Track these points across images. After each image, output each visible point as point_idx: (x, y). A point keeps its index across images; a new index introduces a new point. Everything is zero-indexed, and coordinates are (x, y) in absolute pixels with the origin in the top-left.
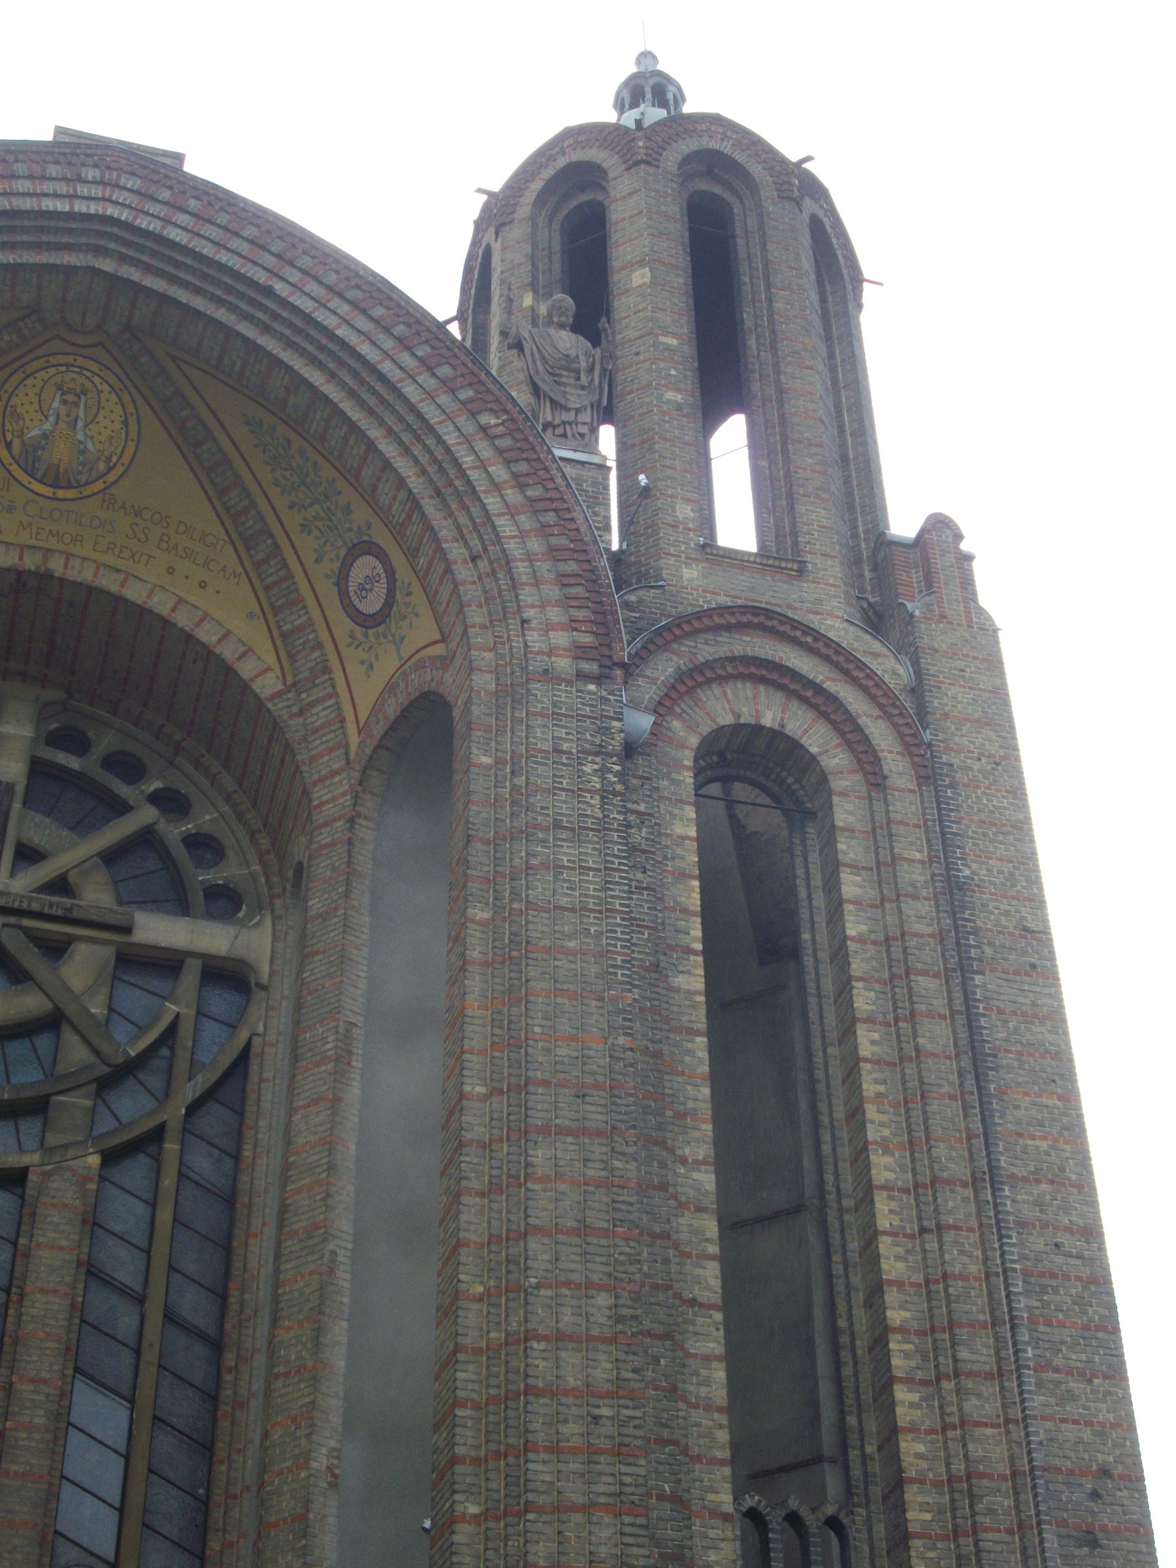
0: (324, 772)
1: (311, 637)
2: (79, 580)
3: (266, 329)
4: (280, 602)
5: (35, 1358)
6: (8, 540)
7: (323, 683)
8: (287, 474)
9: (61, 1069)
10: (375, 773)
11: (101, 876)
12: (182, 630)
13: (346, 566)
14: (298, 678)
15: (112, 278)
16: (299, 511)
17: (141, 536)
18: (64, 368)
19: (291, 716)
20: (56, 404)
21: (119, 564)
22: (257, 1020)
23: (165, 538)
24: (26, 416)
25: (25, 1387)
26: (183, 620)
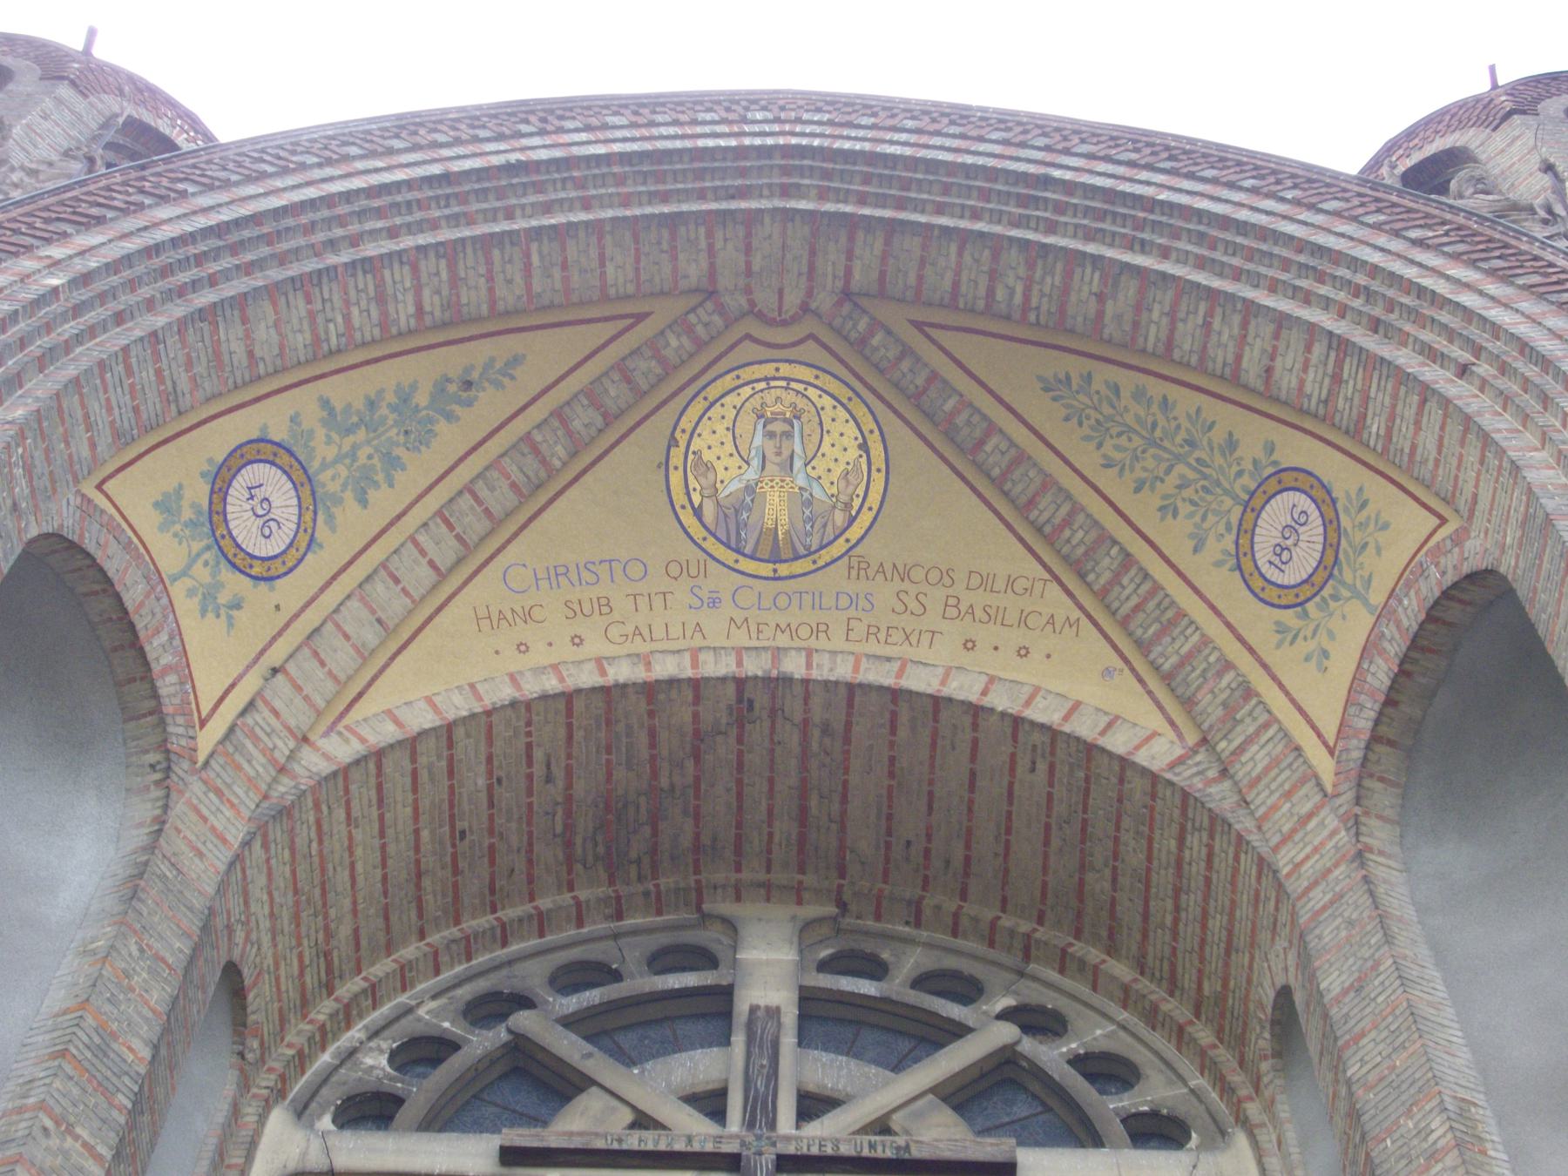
0: (1286, 828)
1: (1212, 659)
2: (832, 678)
3: (1052, 228)
4: (1151, 631)
6: (717, 644)
7: (1250, 714)
8: (1123, 441)
10: (1378, 786)
11: (946, 1115)
12: (1003, 714)
13: (1245, 531)
14: (1205, 726)
16: (1152, 489)
18: (763, 385)
19: (1209, 782)
20: (758, 440)
23: (952, 601)
26: (1000, 701)
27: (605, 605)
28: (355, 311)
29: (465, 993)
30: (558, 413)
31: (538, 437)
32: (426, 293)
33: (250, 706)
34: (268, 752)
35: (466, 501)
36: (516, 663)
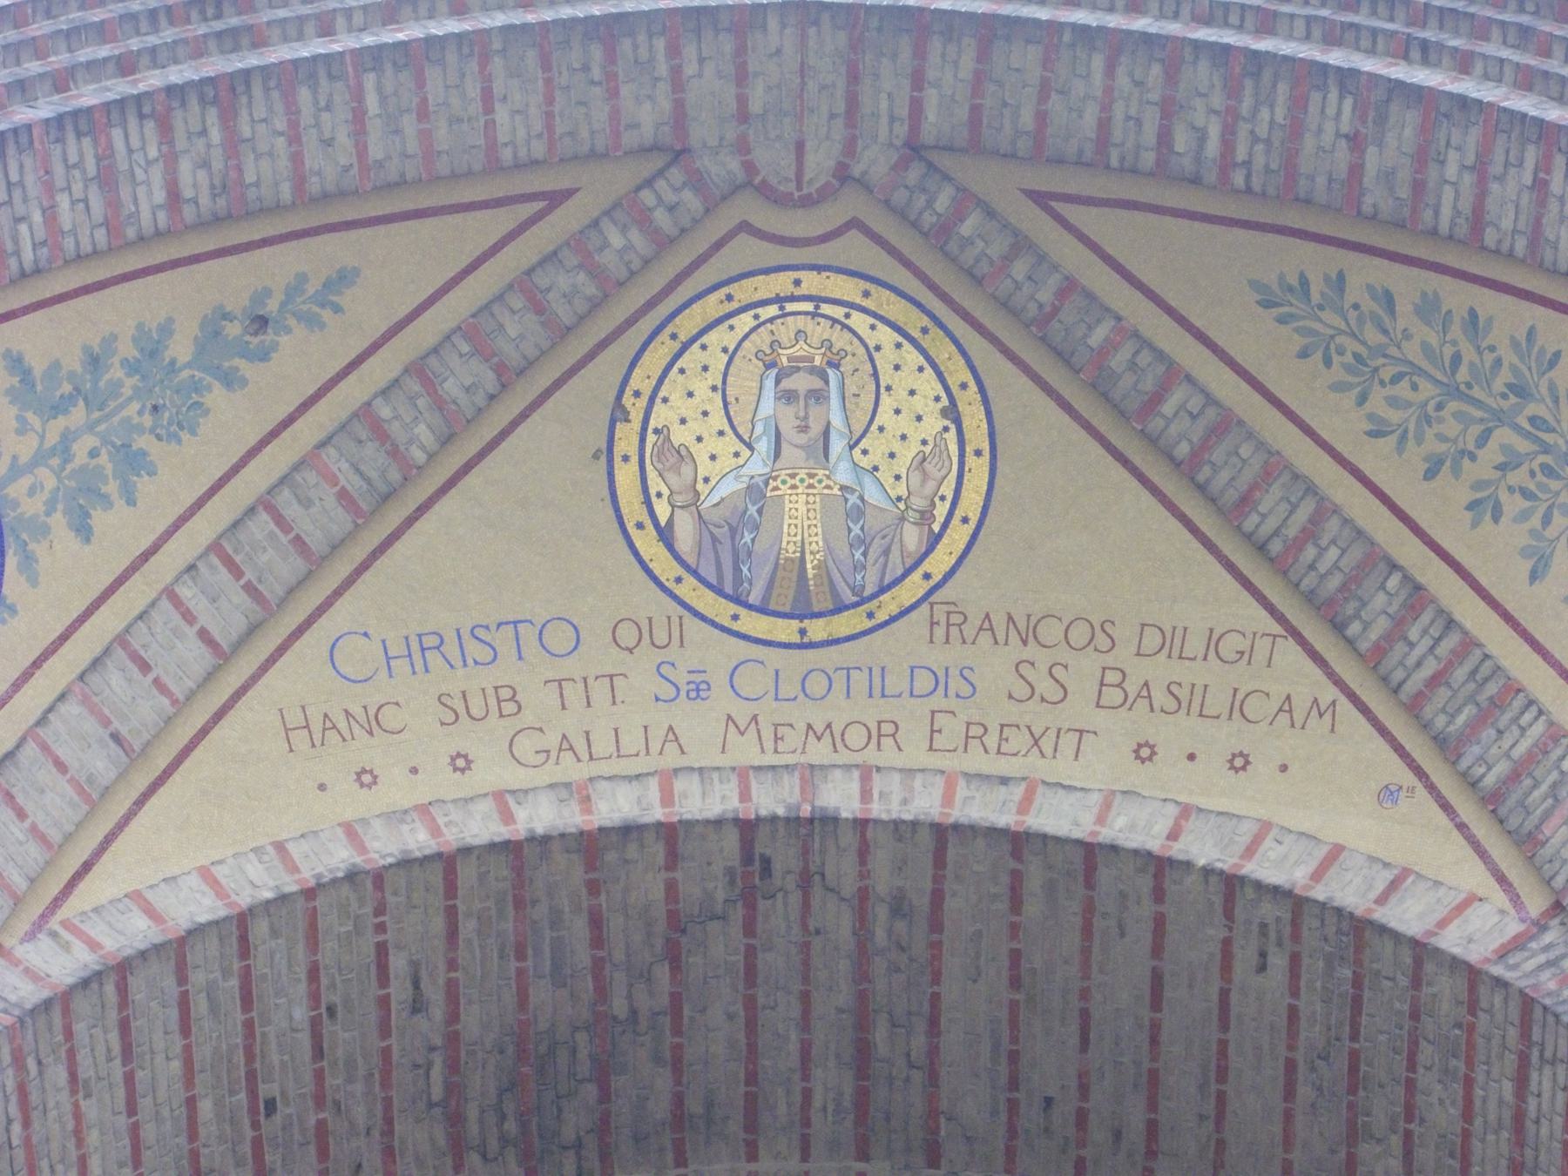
2: (907, 817)
4: (1461, 720)
8: (1403, 390)
12: (1207, 872)
17: (1045, 686)
18: (772, 310)
20: (768, 406)
21: (1003, 766)
23: (1112, 677)
24: (695, 448)
28: (63, 201)
30: (417, 369)
32: (185, 166)
35: (262, 524)
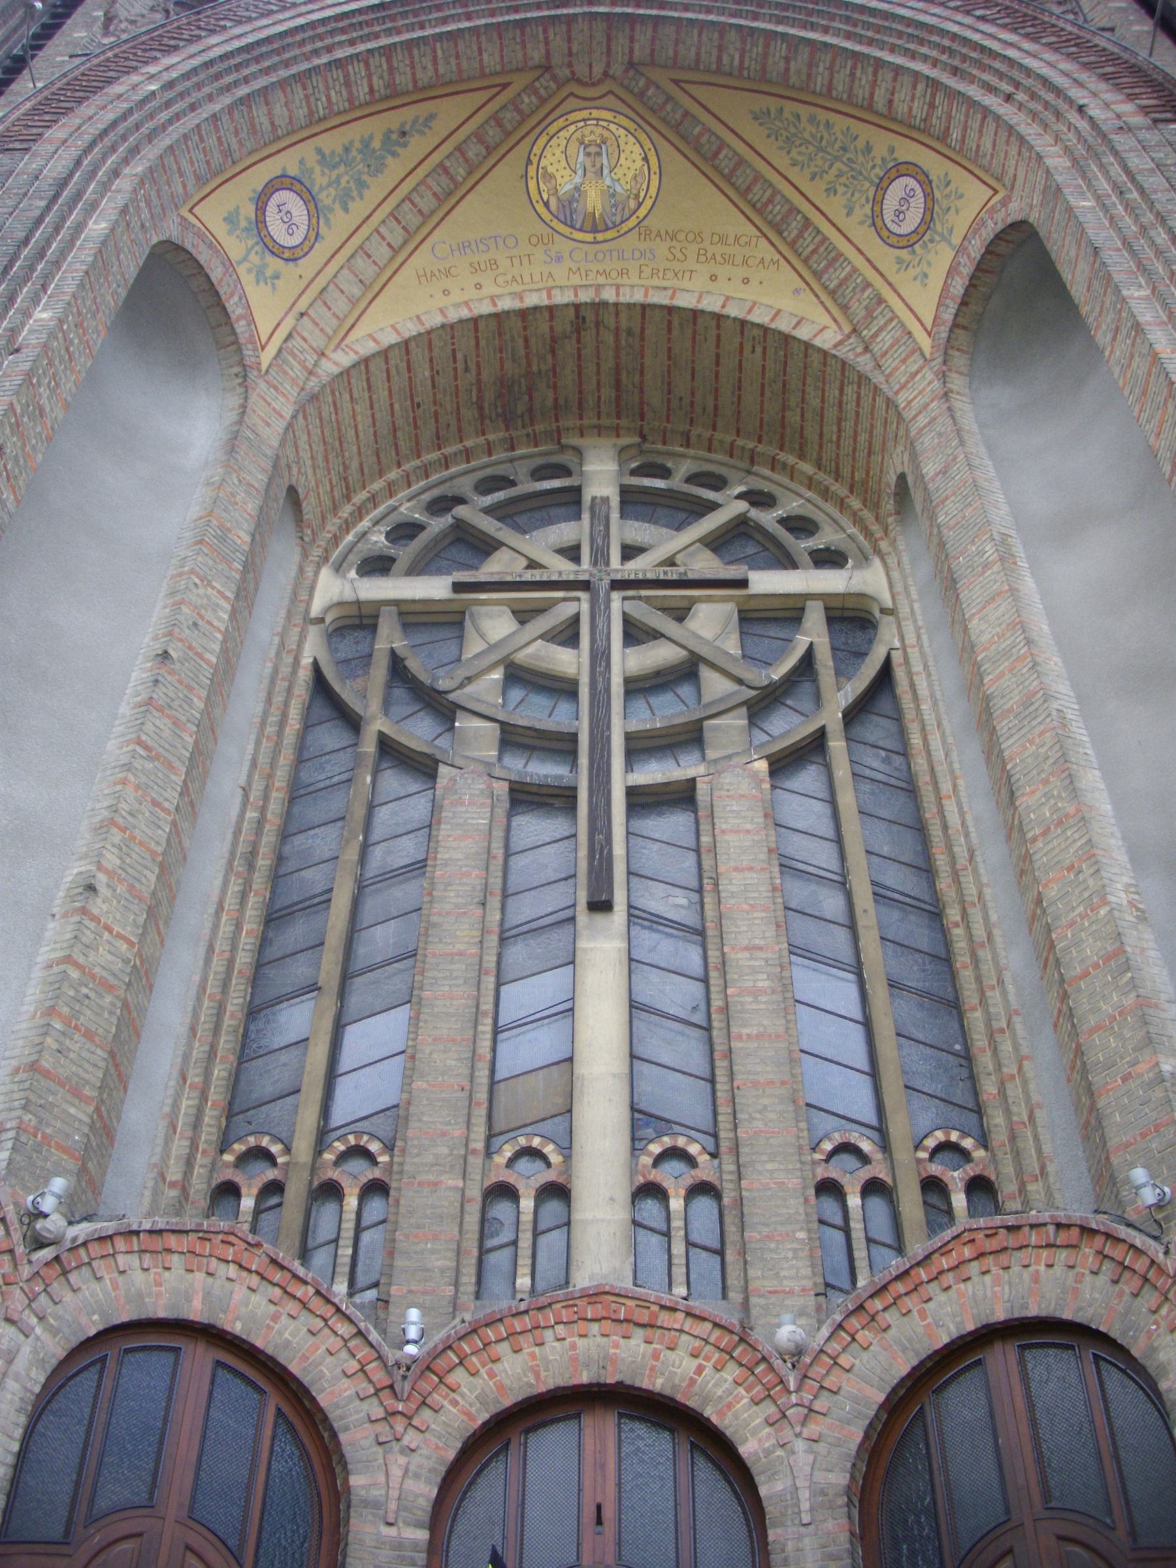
0: (903, 380)
5: (744, 928)
8: (803, 149)
9: (706, 699)
10: (957, 353)
12: (735, 319)
15: (608, 16)
17: (679, 255)
20: (581, 158)
21: (666, 284)
22: (887, 639)
25: (740, 956)
26: (733, 311)
27: (494, 264)
28: (333, 93)
29: (427, 497)
31: (448, 164)
32: (375, 79)
33: (290, 336)
34: (302, 363)
35: (407, 206)
36: (442, 301)
